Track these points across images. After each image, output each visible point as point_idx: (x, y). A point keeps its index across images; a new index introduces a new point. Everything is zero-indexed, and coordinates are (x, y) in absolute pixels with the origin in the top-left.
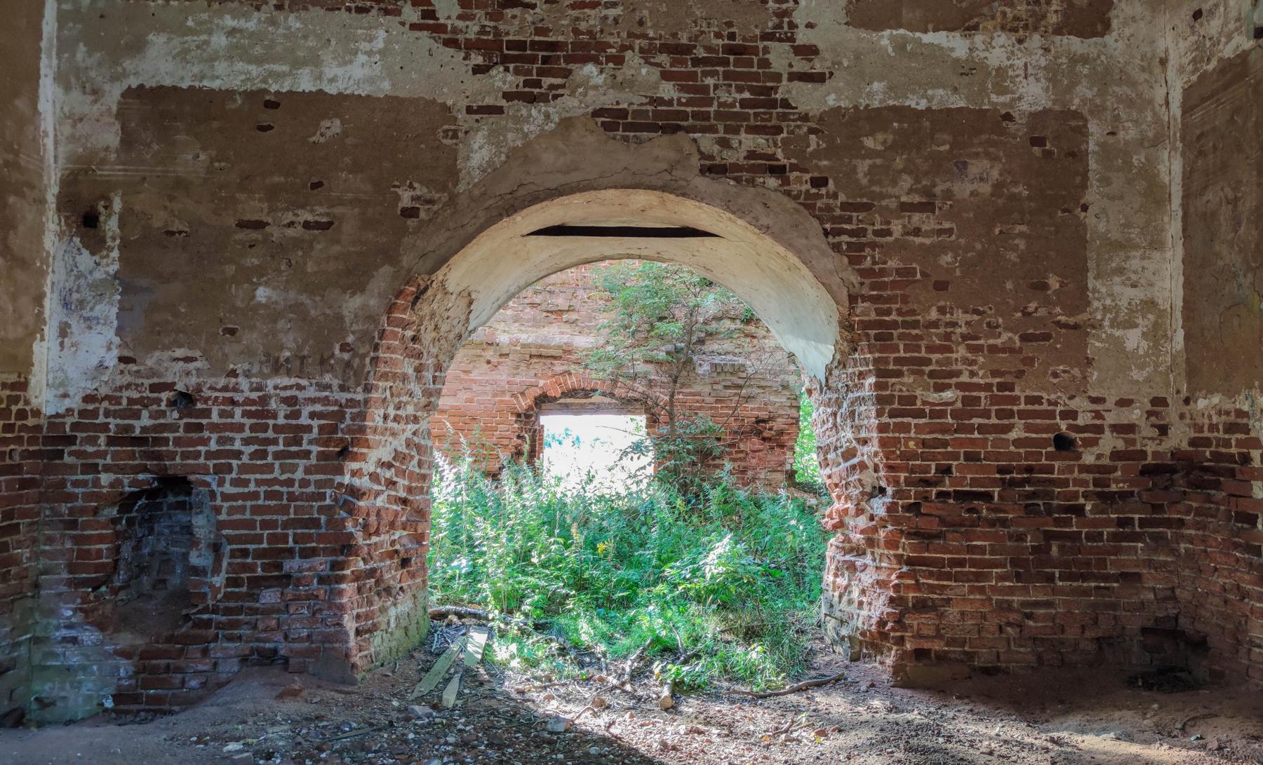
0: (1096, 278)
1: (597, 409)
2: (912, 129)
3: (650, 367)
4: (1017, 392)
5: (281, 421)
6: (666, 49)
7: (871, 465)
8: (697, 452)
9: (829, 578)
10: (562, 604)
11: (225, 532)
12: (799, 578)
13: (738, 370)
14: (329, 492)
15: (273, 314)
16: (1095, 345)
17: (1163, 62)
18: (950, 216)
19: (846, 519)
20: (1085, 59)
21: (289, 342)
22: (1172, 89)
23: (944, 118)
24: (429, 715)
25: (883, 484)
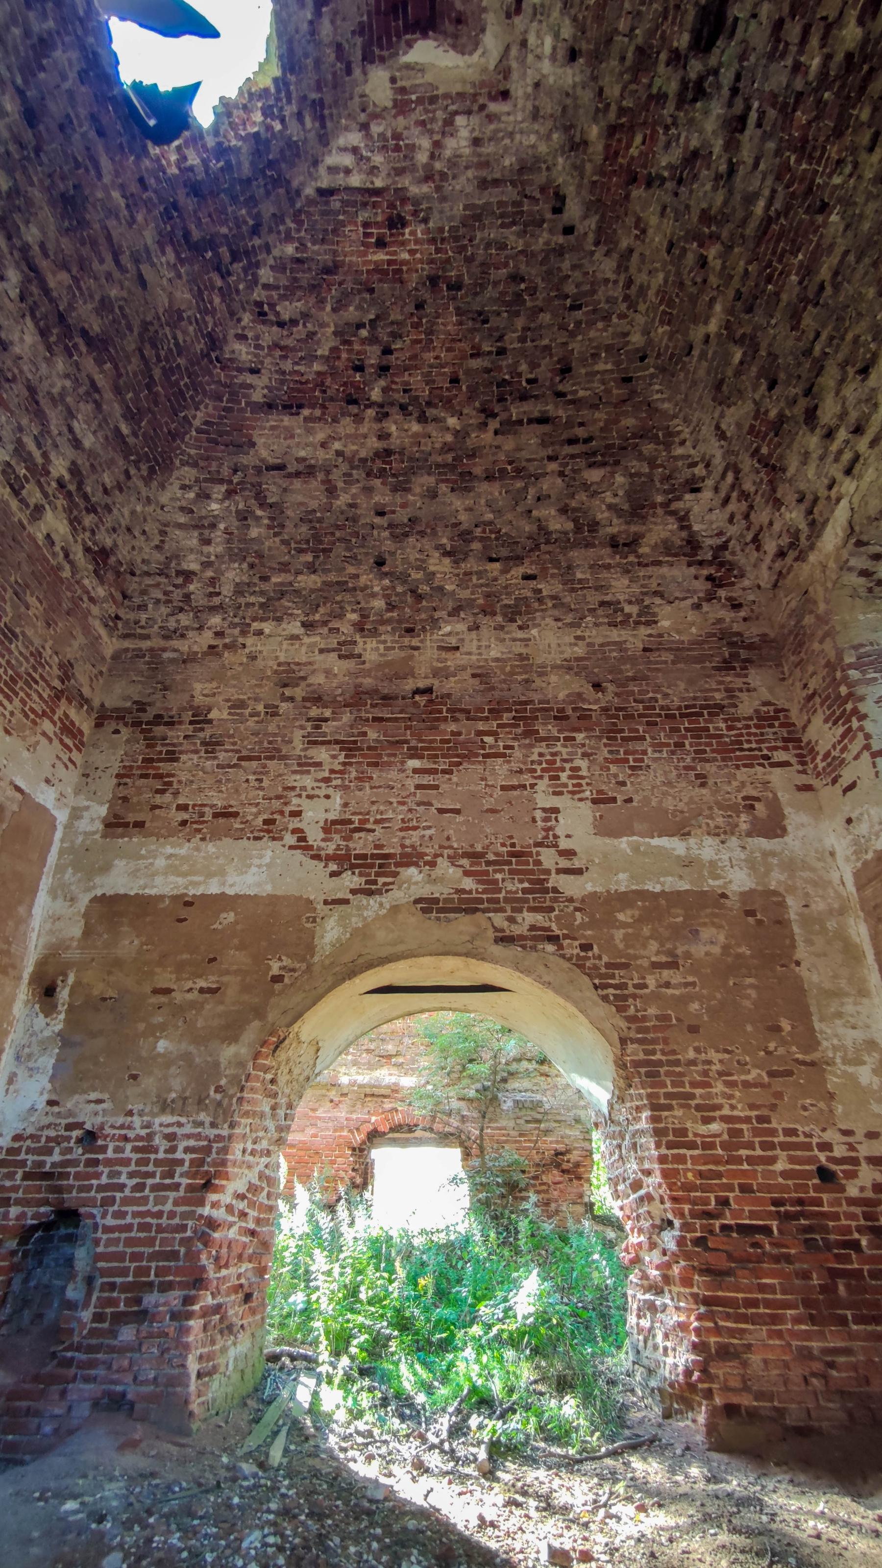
0: (821, 1020)
1: (419, 1142)
2: (654, 907)
3: (462, 1104)
4: (774, 1125)
5: (161, 1155)
6: (466, 855)
7: (656, 1196)
8: (506, 1184)
9: (632, 1319)
10: (386, 1346)
11: (101, 1264)
12: (604, 1317)
13: (536, 1105)
14: (190, 1223)
15: (168, 1061)
16: (833, 1081)
17: (832, 854)
18: (693, 971)
19: (641, 1254)
20: (773, 854)
21: (177, 1084)
22: (844, 873)
23: (675, 898)
24: (255, 1476)
25: (670, 1216)
